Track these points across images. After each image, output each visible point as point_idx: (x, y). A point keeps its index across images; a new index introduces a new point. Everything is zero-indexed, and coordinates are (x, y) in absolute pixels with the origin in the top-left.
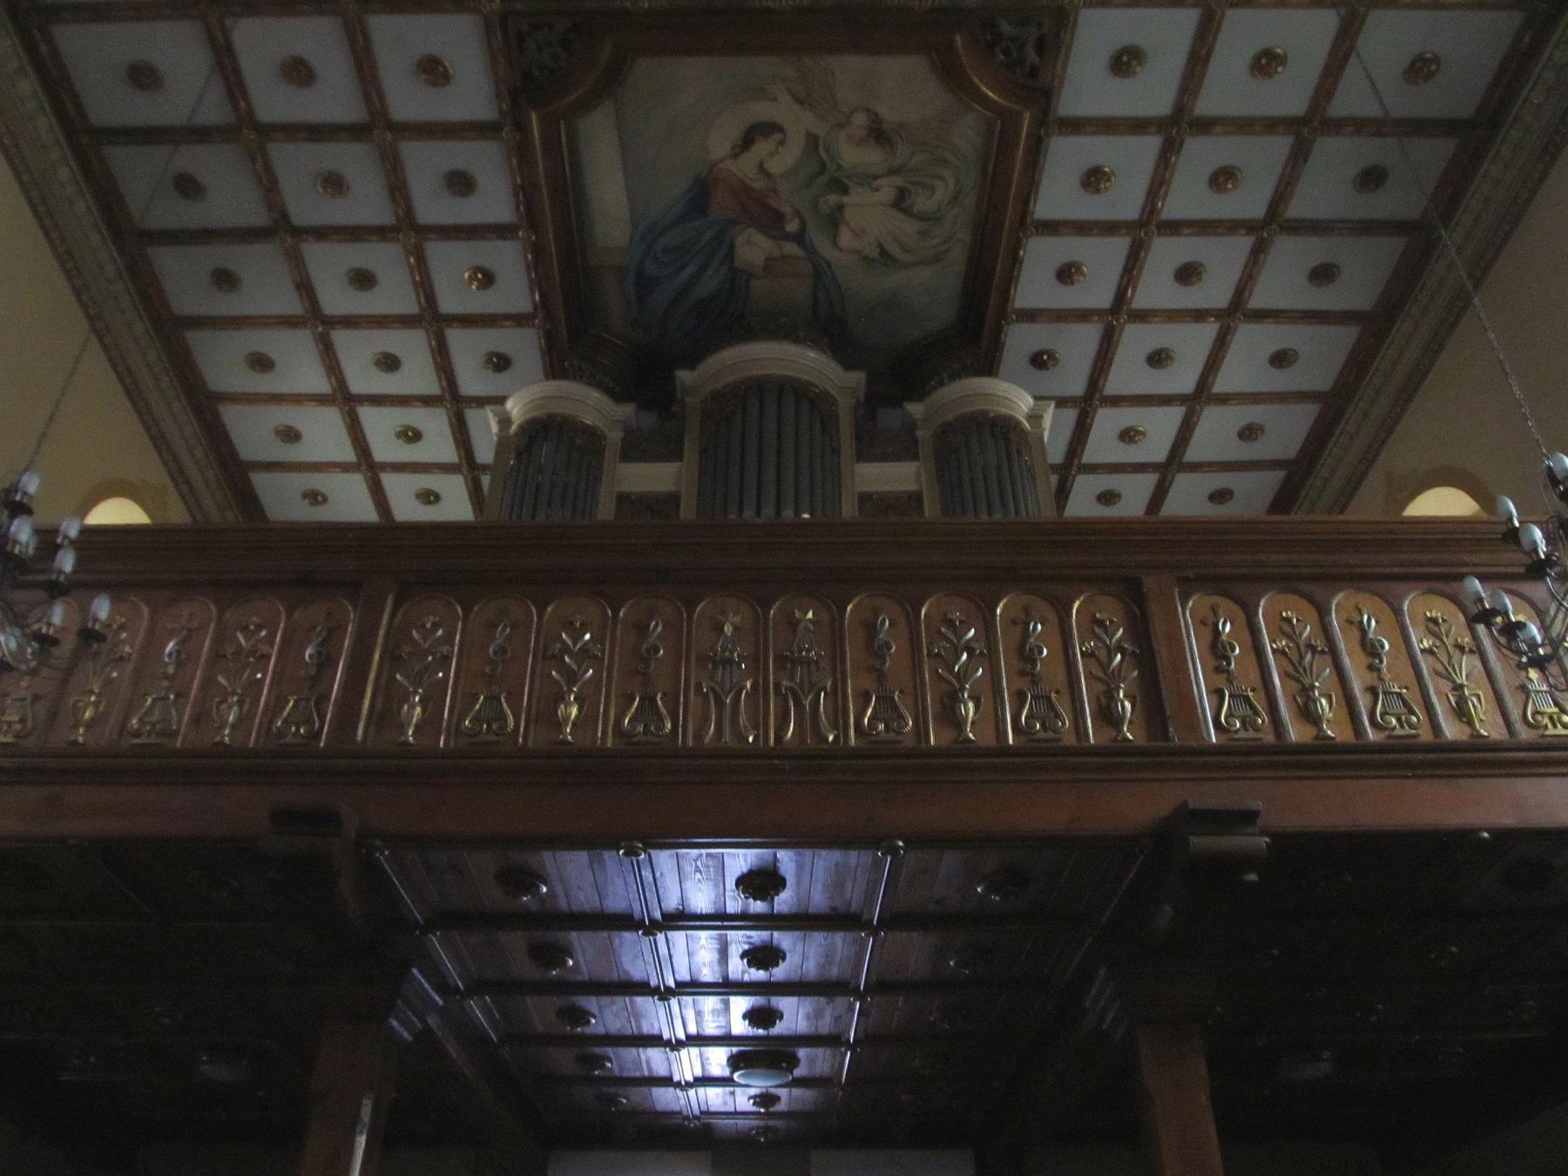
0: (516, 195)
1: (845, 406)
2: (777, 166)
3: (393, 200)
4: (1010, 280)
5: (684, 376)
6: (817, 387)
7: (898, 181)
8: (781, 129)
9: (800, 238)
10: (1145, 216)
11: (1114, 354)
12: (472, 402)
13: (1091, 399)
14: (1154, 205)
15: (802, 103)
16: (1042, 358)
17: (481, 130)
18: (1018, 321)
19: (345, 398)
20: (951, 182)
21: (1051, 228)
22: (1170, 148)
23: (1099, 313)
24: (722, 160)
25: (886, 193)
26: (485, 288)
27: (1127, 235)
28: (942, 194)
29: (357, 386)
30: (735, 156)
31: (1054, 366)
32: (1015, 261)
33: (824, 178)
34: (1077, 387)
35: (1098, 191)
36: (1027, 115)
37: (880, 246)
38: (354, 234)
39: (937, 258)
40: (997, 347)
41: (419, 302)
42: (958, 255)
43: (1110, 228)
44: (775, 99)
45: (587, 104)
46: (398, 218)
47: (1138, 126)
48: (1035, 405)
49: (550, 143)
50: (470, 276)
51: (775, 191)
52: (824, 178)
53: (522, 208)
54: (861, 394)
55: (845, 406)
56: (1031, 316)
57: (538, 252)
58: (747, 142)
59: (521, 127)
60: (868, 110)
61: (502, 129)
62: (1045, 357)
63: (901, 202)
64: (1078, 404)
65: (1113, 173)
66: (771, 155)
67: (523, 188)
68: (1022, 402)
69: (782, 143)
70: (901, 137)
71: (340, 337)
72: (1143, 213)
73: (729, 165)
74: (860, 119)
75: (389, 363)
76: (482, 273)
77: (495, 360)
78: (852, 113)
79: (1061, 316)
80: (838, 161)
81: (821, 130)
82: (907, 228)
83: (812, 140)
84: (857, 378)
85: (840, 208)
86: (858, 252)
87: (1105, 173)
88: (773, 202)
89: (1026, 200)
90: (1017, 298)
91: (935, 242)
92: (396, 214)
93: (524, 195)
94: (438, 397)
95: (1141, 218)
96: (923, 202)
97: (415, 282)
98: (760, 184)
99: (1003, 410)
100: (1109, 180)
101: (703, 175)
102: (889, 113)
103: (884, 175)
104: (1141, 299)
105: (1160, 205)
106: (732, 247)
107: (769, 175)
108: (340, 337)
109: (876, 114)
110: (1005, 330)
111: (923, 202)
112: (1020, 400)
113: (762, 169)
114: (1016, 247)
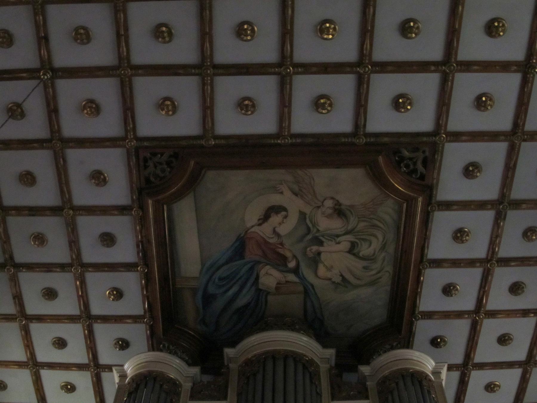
0: (138, 246)
1: (324, 368)
2: (283, 230)
3: (71, 249)
4: (416, 294)
5: (229, 352)
6: (307, 357)
7: (350, 238)
8: (285, 209)
9: (296, 271)
10: (490, 255)
11: (478, 337)
12: (105, 368)
13: (467, 365)
14: (494, 250)
15: (296, 194)
16: (437, 341)
17: (122, 210)
18: (422, 318)
19: (34, 364)
20: (381, 238)
21: (438, 263)
22: (500, 217)
23: (468, 313)
24: (253, 226)
25: (345, 245)
26: (117, 300)
27: (480, 267)
28: (376, 245)
29: (41, 357)
30: (260, 225)
31: (444, 345)
32: (418, 282)
33: (309, 237)
34: (459, 359)
35: (463, 242)
36: (420, 199)
37: (342, 275)
38: (48, 268)
39: (372, 283)
40: (411, 334)
41: (89, 358)
42: (386, 279)
43: (471, 263)
44: (282, 193)
45: (179, 195)
46: (72, 259)
47: (481, 205)
48: (435, 366)
49: (158, 212)
50: (109, 293)
51: (282, 244)
52: (309, 237)
53: (141, 254)
54: (333, 363)
55: (324, 368)
56: (429, 315)
57: (148, 277)
58: (266, 217)
59: (142, 207)
60: (332, 198)
61: (132, 209)
62: (439, 340)
63: (352, 250)
64: (460, 369)
65: (470, 232)
66: (280, 224)
67: (142, 242)
68: (429, 364)
69: (286, 217)
70: (352, 213)
71: (34, 327)
72: (488, 255)
73: (256, 229)
74: (329, 203)
75: (61, 343)
76: (116, 291)
77: (120, 343)
78: (325, 199)
79: (447, 315)
80: (318, 227)
81: (307, 210)
82: (357, 265)
83: (303, 215)
84: (330, 353)
85: (319, 254)
86: (330, 279)
87: (465, 231)
88: (281, 251)
89: (423, 249)
90: (420, 306)
91: (374, 272)
92: (72, 257)
93: (142, 246)
94: (87, 364)
95: (487, 258)
96: (365, 250)
97: (79, 296)
98: (273, 240)
99: (418, 368)
100: (468, 235)
101: (242, 235)
102: (345, 201)
103: (344, 234)
104: (491, 304)
105: (497, 249)
106: (257, 278)
107: (278, 235)
108: (34, 327)
109: (338, 201)
110: (415, 324)
111: (365, 250)
112: (427, 363)
113: (274, 231)
114: (419, 274)
